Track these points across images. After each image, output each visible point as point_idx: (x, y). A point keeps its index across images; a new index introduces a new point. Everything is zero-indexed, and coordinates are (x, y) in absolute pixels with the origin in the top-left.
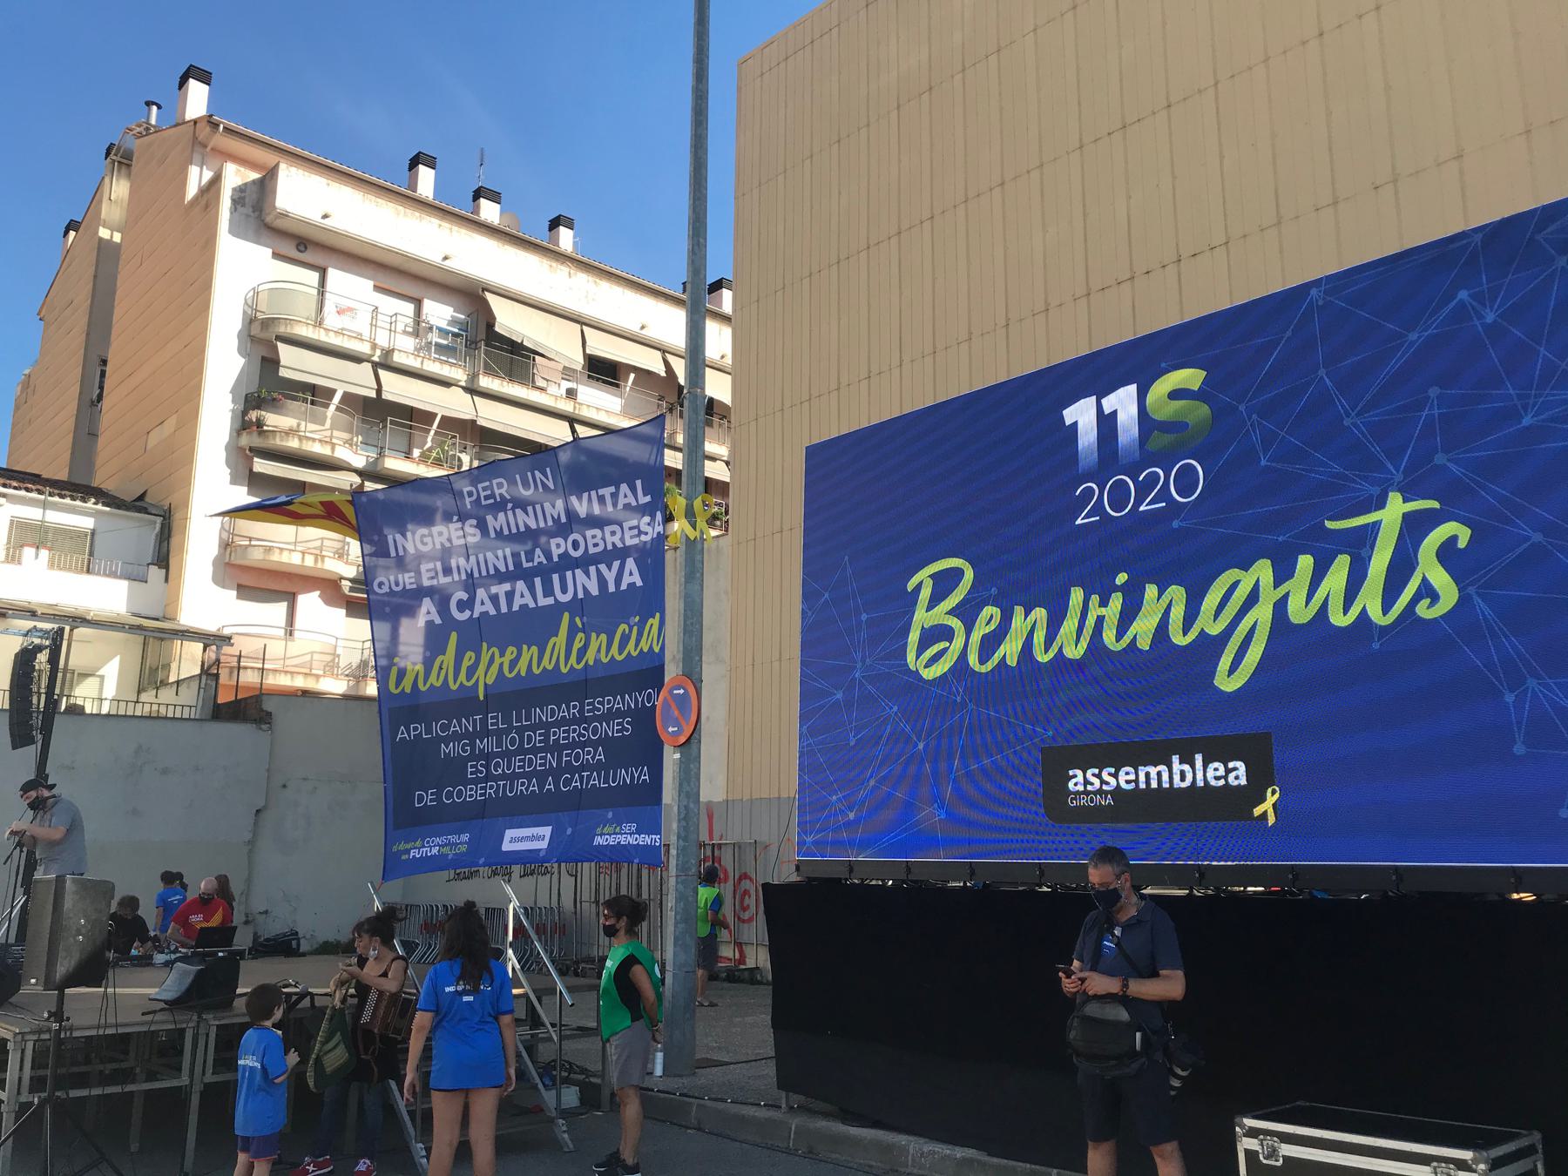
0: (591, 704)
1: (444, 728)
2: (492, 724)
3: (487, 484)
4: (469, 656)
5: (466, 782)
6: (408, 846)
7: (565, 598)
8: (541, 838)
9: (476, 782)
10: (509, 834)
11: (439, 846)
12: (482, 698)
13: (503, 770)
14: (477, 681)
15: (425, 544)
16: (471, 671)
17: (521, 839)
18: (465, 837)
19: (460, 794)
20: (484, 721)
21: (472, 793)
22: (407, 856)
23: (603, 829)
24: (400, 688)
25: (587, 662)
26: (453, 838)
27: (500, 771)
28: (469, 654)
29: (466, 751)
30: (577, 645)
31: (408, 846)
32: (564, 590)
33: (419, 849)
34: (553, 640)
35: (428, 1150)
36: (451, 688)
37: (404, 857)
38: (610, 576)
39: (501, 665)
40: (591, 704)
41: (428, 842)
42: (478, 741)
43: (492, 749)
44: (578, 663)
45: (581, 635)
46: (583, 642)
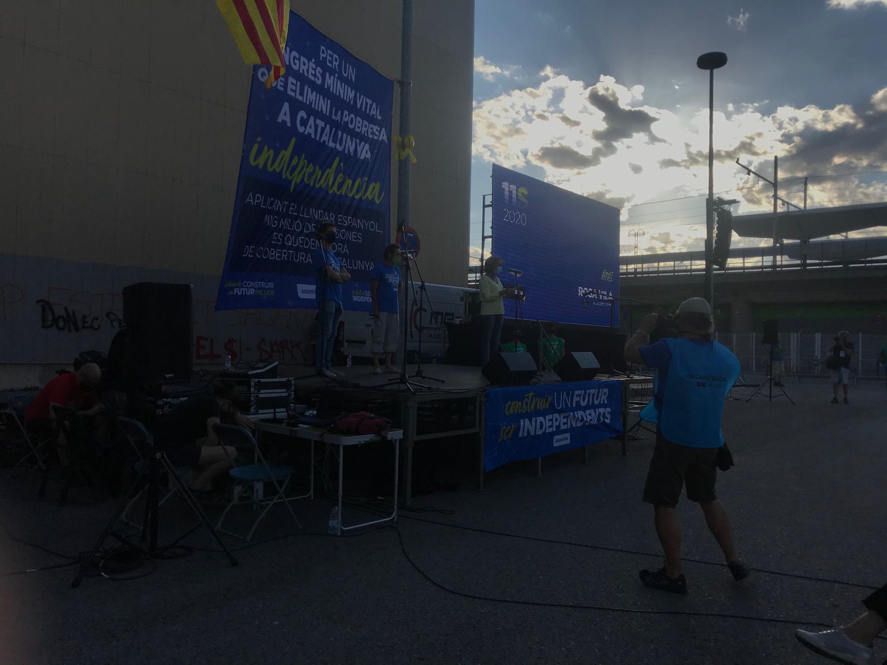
0: (342, 218)
8: (567, 439)
9: (276, 247)
10: (568, 442)
11: (255, 288)
17: (560, 440)
18: (271, 285)
19: (266, 253)
21: (274, 255)
22: (232, 292)
24: (256, 162)
25: (341, 193)
26: (263, 284)
27: (290, 244)
30: (339, 180)
39: (305, 173)
40: (342, 218)
45: (341, 175)
46: (342, 180)
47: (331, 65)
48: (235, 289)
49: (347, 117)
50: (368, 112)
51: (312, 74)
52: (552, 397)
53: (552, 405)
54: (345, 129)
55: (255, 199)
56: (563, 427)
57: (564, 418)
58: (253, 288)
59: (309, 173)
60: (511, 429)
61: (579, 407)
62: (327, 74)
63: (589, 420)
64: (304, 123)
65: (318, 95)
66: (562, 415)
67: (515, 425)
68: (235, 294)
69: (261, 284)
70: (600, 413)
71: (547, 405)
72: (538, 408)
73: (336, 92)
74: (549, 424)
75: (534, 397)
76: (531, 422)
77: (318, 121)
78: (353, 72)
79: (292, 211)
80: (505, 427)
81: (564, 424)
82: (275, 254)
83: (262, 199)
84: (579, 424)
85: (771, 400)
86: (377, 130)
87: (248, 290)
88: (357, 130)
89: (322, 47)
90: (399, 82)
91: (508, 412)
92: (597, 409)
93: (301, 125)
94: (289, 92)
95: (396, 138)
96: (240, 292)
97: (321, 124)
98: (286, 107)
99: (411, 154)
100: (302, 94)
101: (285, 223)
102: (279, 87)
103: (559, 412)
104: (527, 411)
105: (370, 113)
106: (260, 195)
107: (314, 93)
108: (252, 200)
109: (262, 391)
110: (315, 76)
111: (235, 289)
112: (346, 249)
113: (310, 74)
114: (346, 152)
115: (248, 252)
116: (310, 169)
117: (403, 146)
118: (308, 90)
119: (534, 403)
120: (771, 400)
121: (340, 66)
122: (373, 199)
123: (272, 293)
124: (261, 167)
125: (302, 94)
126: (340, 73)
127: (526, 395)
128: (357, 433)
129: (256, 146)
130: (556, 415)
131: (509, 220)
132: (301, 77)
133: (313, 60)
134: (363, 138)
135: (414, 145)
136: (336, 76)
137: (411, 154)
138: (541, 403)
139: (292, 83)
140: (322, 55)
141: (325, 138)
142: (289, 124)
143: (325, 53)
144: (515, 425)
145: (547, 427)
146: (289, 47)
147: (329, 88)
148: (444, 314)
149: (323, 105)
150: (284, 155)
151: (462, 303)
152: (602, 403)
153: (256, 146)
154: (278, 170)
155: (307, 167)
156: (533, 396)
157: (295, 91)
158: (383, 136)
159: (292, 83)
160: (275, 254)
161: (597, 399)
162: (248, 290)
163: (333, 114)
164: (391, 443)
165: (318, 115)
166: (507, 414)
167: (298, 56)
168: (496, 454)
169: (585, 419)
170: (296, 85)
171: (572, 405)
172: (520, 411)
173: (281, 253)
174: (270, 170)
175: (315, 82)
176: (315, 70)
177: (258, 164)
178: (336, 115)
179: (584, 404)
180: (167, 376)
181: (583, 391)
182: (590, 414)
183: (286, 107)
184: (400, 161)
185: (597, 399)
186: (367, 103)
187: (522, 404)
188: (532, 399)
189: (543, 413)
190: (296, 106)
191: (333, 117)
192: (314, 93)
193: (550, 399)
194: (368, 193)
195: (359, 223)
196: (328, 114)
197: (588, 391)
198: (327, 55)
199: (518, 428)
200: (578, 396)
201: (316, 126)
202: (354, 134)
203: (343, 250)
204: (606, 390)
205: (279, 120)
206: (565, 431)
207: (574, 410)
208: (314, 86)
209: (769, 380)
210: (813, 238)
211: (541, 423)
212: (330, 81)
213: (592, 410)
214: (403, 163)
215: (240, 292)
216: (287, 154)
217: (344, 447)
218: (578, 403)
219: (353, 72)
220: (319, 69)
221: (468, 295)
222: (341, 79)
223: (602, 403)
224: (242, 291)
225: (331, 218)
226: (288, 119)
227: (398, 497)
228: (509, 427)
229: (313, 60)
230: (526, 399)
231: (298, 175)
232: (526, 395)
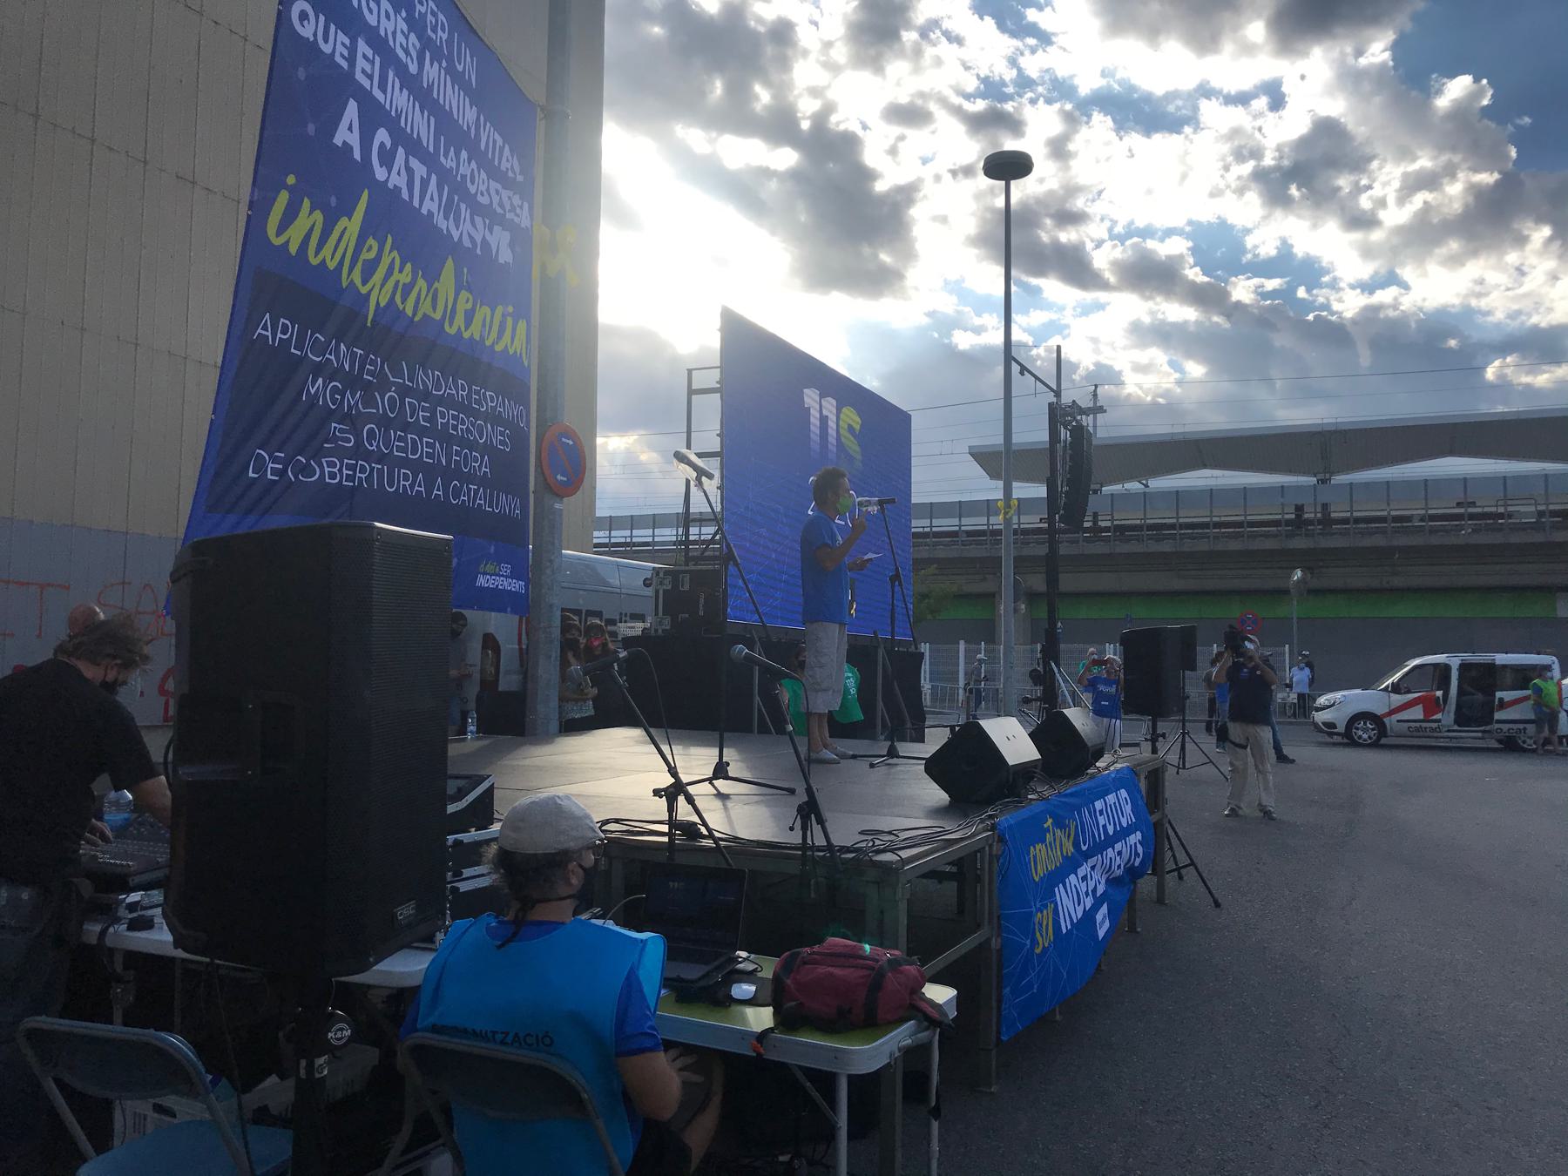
13: (378, 446)
28: (371, 241)
39: (398, 282)
45: (464, 294)
59: (404, 284)
64: (387, 159)
73: (444, 101)
77: (415, 163)
78: (472, 64)
79: (370, 373)
82: (340, 470)
85: (1178, 773)
94: (359, 76)
97: (420, 169)
105: (421, 205)
106: (287, 322)
107: (405, 92)
108: (269, 334)
109: (467, 872)
112: (486, 467)
121: (450, 41)
124: (293, 249)
125: (383, 89)
129: (283, 198)
133: (404, 14)
141: (429, 206)
148: (584, 612)
151: (650, 592)
153: (283, 198)
154: (332, 265)
160: (340, 470)
163: (442, 154)
165: (414, 147)
170: (372, 63)
173: (352, 468)
174: (314, 261)
177: (288, 242)
180: (781, 1158)
183: (352, 109)
190: (373, 116)
201: (409, 171)
210: (1110, 483)
216: (351, 225)
217: (850, 1077)
219: (472, 64)
220: (413, 37)
221: (661, 575)
225: (460, 392)
226: (354, 140)
227: (849, 1139)
231: (382, 286)
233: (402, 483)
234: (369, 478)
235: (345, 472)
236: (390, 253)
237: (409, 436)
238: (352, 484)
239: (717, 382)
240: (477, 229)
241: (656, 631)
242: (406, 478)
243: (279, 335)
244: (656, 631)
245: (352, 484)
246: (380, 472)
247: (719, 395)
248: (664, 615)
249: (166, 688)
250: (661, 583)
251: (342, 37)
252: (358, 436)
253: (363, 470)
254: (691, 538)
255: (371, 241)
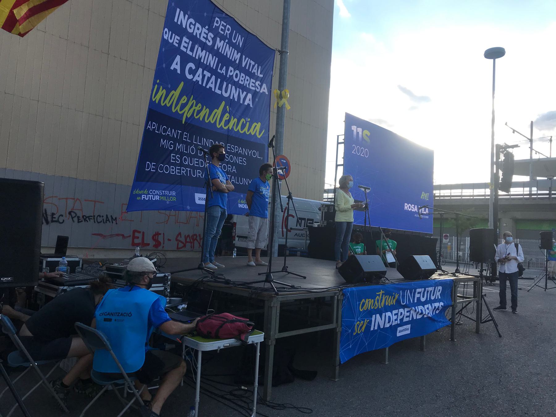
1: (165, 131)
2: (185, 138)
3: (225, 24)
4: (185, 98)
5: (170, 164)
6: (141, 192)
7: (226, 95)
8: (407, 329)
9: (175, 165)
10: (408, 332)
11: (160, 196)
12: (183, 123)
13: (188, 163)
14: (184, 112)
15: (190, 28)
16: (183, 106)
18: (174, 193)
19: (167, 169)
20: (182, 135)
21: (174, 171)
23: (240, 201)
24: (209, 120)
25: (229, 127)
26: (167, 192)
27: (187, 163)
28: (185, 97)
29: (171, 147)
31: (141, 192)
32: (226, 92)
33: (147, 195)
34: (216, 110)
35: (497, 248)
36: (212, 122)
37: (138, 198)
38: (242, 96)
39: (194, 110)
41: (151, 192)
42: (177, 144)
43: (183, 151)
44: (225, 126)
45: (227, 115)
47: (223, 33)
48: (143, 196)
49: (233, 72)
50: (250, 70)
51: (204, 37)
52: (398, 295)
53: (398, 301)
54: (230, 80)
55: (153, 126)
56: (406, 320)
57: (407, 312)
58: (158, 195)
60: (364, 323)
61: (419, 303)
62: (218, 39)
63: (427, 314)
65: (208, 53)
66: (406, 310)
67: (367, 320)
68: (142, 199)
69: (165, 192)
70: (435, 307)
71: (394, 301)
72: (387, 304)
74: (395, 317)
75: (384, 295)
76: (381, 317)
77: (205, 72)
78: (241, 41)
80: (358, 322)
81: (407, 317)
83: (156, 125)
84: (419, 317)
86: (259, 84)
87: (154, 196)
88: (240, 82)
89: (217, 19)
90: (279, 51)
91: (362, 309)
92: (433, 304)
93: (190, 74)
94: (182, 48)
95: (275, 91)
96: (147, 198)
97: (207, 74)
98: (178, 58)
99: (286, 103)
100: (192, 50)
101: (179, 146)
102: (175, 44)
103: (404, 307)
104: (378, 307)
110: (206, 39)
111: (143, 196)
113: (202, 37)
114: (231, 98)
115: (151, 167)
116: (198, 108)
117: (280, 97)
118: (198, 49)
119: (383, 301)
120: (545, 291)
121: (231, 34)
122: (255, 134)
123: (174, 199)
126: (230, 40)
127: (377, 293)
128: (217, 337)
130: (401, 310)
131: (364, 155)
132: (194, 39)
133: (207, 27)
134: (244, 88)
135: (288, 96)
136: (227, 41)
137: (286, 103)
138: (390, 299)
139: (185, 42)
140: (215, 24)
142: (179, 72)
143: (218, 23)
144: (367, 320)
145: (394, 320)
146: (188, 15)
147: (218, 49)
148: (306, 219)
149: (212, 61)
150: (174, 94)
152: (437, 298)
154: (168, 105)
155: (196, 106)
156: (383, 294)
157: (187, 48)
158: (264, 89)
159: (185, 42)
161: (433, 295)
162: (154, 196)
164: (253, 346)
165: (206, 68)
166: (361, 310)
167: (194, 23)
168: (350, 347)
169: (424, 313)
170: (188, 44)
171: (414, 300)
172: (372, 308)
173: (180, 169)
175: (205, 43)
176: (207, 34)
178: (221, 69)
179: (423, 300)
181: (423, 289)
182: (428, 308)
183: (178, 58)
184: (278, 107)
185: (433, 295)
186: (250, 64)
187: (374, 301)
188: (382, 296)
189: (390, 309)
190: (186, 59)
191: (219, 71)
192: (204, 51)
193: (397, 297)
194: (251, 130)
195: (245, 152)
196: (214, 68)
197: (427, 289)
198: (220, 25)
199: (370, 322)
200: (419, 293)
201: (204, 76)
202: (237, 85)
203: (232, 170)
204: (440, 288)
205: (172, 68)
206: (407, 323)
207: (415, 305)
208: (204, 46)
209: (545, 276)
211: (389, 317)
212: (219, 44)
213: (430, 304)
214: (280, 110)
215: (147, 198)
217: (203, 352)
218: (419, 299)
222: (231, 44)
223: (437, 298)
224: (149, 197)
226: (178, 68)
228: (362, 322)
229: (207, 27)
230: (378, 297)
232: (377, 293)
233: (198, 174)
234: (186, 172)
235: (177, 171)
236: (192, 100)
237: (200, 160)
238: (180, 174)
239: (343, 140)
240: (162, 91)
241: (322, 226)
242: (199, 173)
243: (152, 127)
244: (322, 226)
245: (180, 174)
246: (190, 171)
247: (343, 144)
248: (324, 220)
249: (178, 239)
250: (324, 210)
251: (177, 37)
252: (181, 160)
253: (183, 170)
254: (533, 192)
255: (185, 97)
